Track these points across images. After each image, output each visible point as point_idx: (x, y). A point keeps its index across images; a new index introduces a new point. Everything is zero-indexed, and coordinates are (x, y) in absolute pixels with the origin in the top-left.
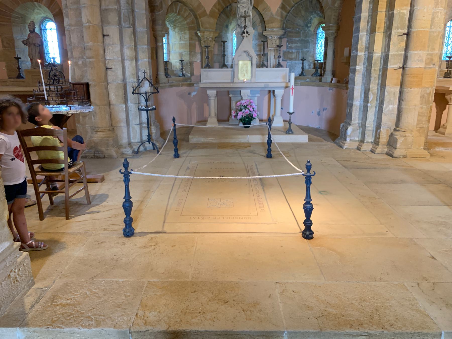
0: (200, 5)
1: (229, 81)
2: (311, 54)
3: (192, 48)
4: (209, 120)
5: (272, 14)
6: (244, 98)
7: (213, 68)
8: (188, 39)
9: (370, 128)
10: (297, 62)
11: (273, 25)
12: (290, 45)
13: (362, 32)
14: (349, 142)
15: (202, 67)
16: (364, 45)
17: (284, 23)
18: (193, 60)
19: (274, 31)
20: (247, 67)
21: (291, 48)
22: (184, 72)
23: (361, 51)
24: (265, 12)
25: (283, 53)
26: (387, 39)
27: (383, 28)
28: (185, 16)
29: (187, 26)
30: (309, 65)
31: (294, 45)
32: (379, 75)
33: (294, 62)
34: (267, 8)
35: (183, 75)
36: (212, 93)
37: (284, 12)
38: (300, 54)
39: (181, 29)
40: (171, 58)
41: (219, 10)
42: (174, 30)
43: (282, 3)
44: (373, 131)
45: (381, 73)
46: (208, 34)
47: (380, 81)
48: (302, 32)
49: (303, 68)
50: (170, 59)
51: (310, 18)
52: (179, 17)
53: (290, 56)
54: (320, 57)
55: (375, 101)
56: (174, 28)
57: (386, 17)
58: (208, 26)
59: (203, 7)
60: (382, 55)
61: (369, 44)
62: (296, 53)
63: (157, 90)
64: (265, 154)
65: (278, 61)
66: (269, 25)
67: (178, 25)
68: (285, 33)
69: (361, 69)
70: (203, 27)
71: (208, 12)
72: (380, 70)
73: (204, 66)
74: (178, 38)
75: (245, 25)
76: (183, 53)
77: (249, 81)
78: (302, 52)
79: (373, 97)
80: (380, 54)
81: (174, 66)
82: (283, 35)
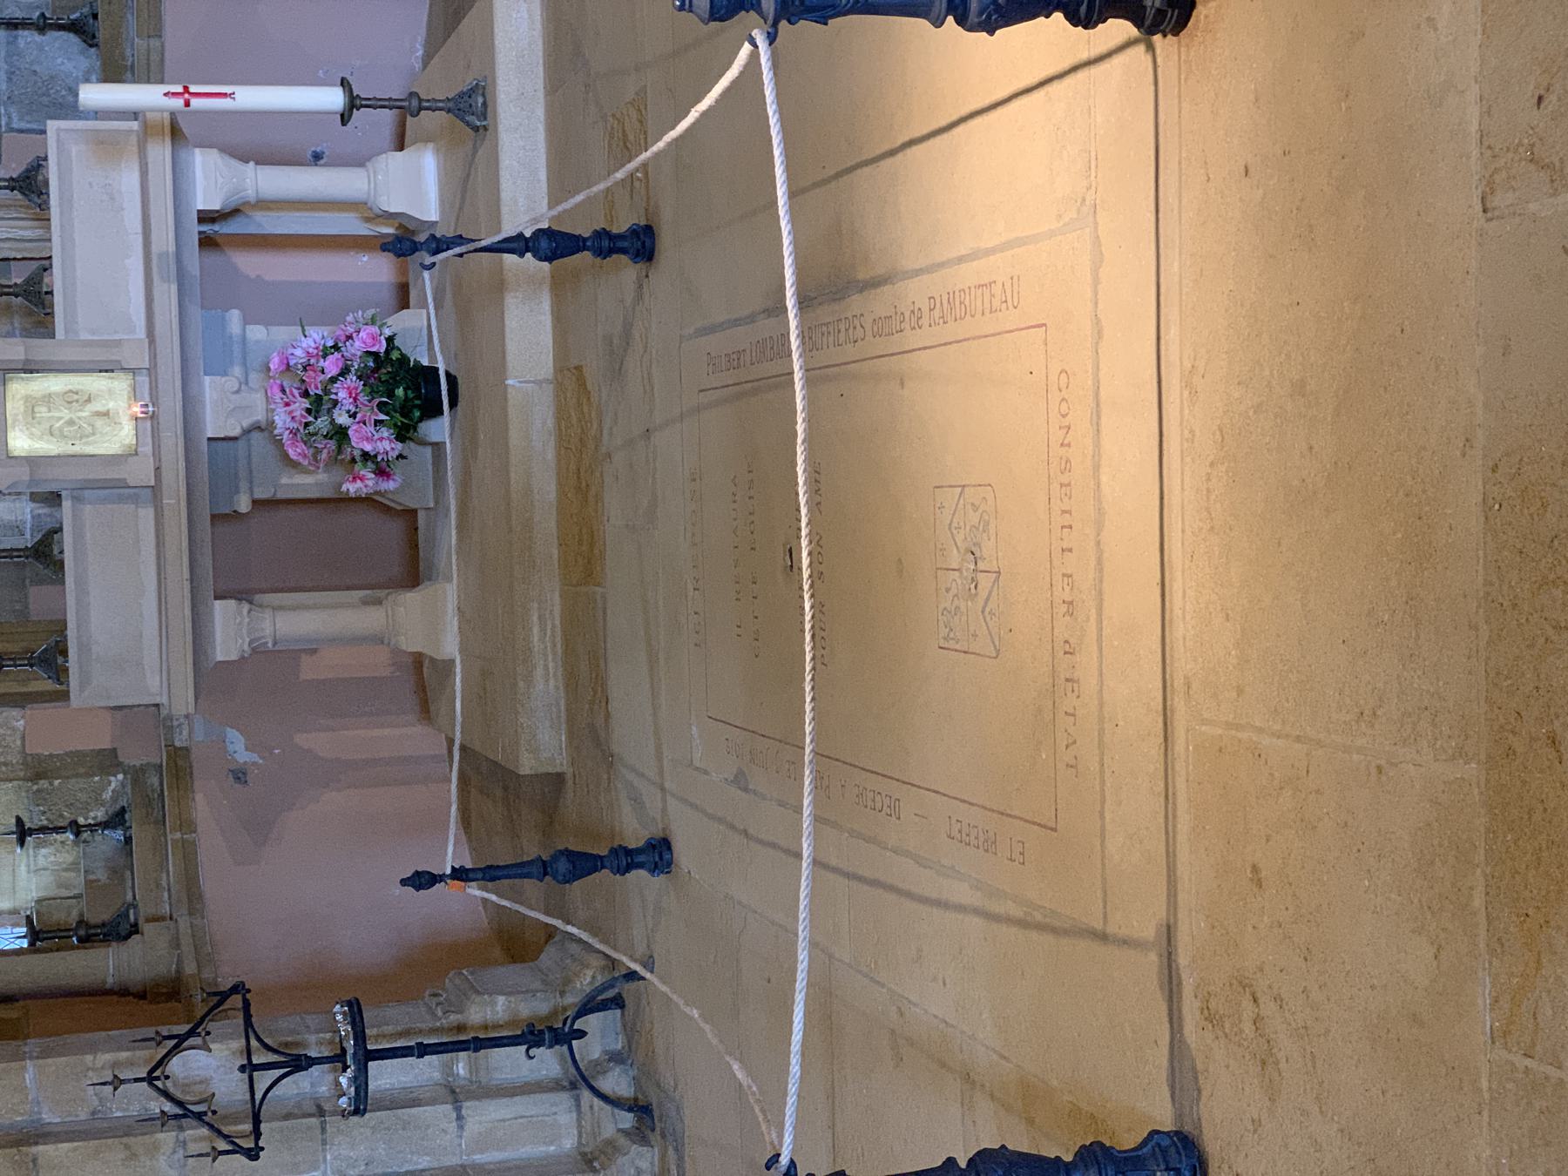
1: (147, 515)
6: (260, 416)
7: (63, 625)
15: (64, 696)
18: (14, 758)
20: (48, 399)
22: (99, 814)
35: (117, 819)
36: (231, 632)
50: (14, 912)
63: (224, 996)
64: (625, 270)
73: (49, 685)
77: (143, 379)
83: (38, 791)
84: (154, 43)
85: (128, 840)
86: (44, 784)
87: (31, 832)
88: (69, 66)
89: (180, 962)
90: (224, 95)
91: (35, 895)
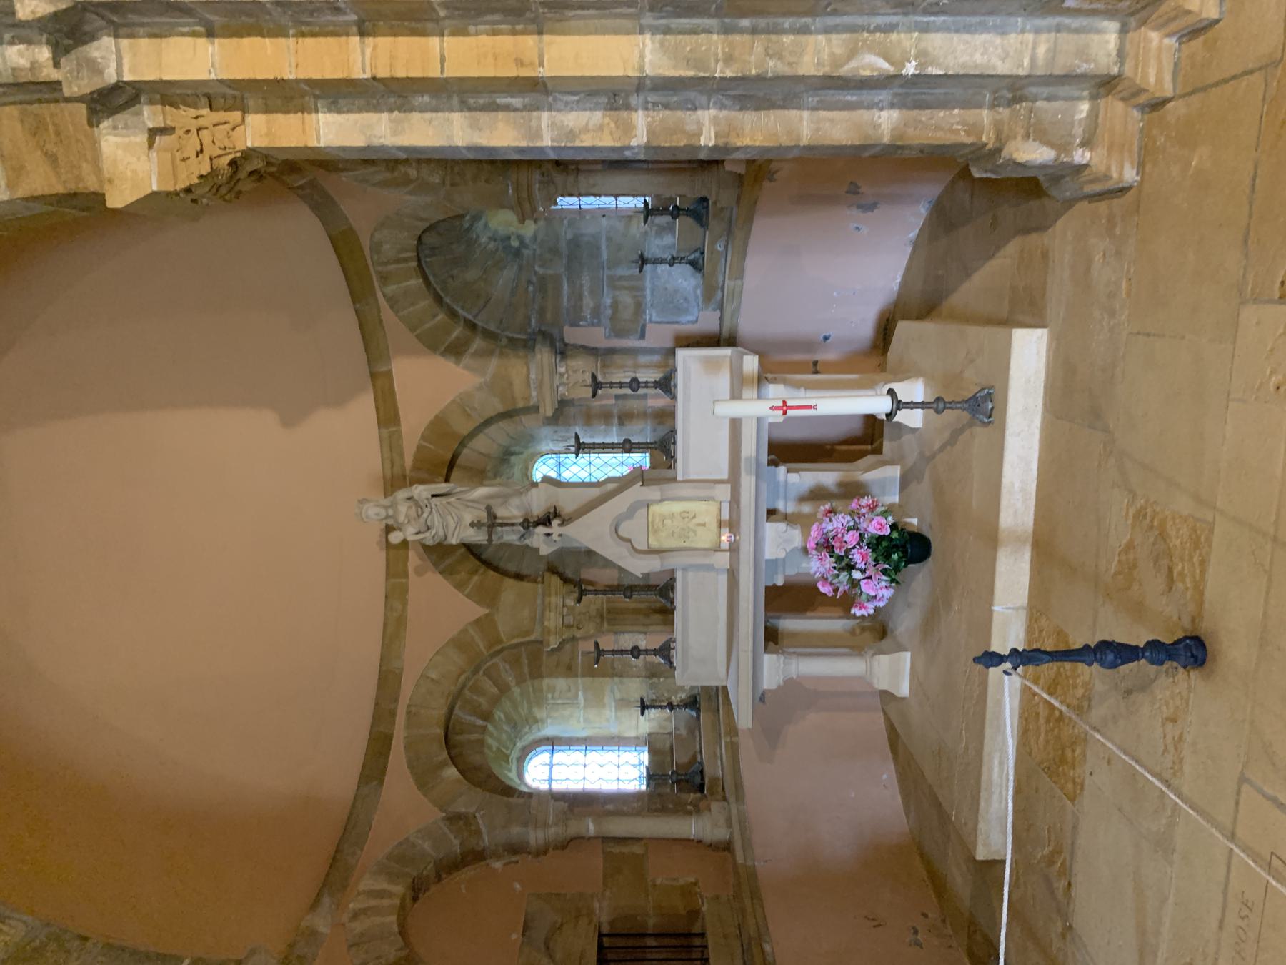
0: (460, 643)
2: (620, 226)
3: (600, 664)
5: (480, 388)
8: (570, 680)
9: (1042, 50)
10: (648, 284)
13: (538, 134)
14: (1102, 151)
16: (597, 117)
17: (511, 340)
19: (537, 376)
21: (596, 312)
23: (629, 128)
26: (571, 13)
27: (519, 38)
28: (495, 690)
29: (529, 683)
30: (662, 230)
31: (588, 302)
32: (754, 31)
34: (462, 404)
37: (472, 350)
38: (622, 271)
39: (539, 700)
40: (632, 734)
41: (475, 572)
42: (543, 721)
43: (443, 354)
44: (1058, 29)
45: (745, 23)
46: (552, 614)
47: (787, 23)
48: (540, 271)
49: (672, 262)
51: (492, 245)
52: (499, 714)
53: (627, 314)
54: (632, 203)
55: (894, 36)
56: (536, 721)
57: (464, 33)
58: (526, 613)
59: (464, 631)
60: (654, 30)
61: (592, 94)
62: (615, 288)
64: (1174, 684)
65: (651, 391)
67: (524, 711)
69: (715, 121)
70: (528, 633)
71: (482, 611)
72: (727, 30)
76: (618, 696)
78: (613, 263)
79: (871, 49)
80: (648, 36)
81: (661, 727)
82: (553, 345)
84: (739, 282)
86: (655, 680)
87: (648, 707)
88: (685, 284)
89: (731, 834)
90: (810, 407)
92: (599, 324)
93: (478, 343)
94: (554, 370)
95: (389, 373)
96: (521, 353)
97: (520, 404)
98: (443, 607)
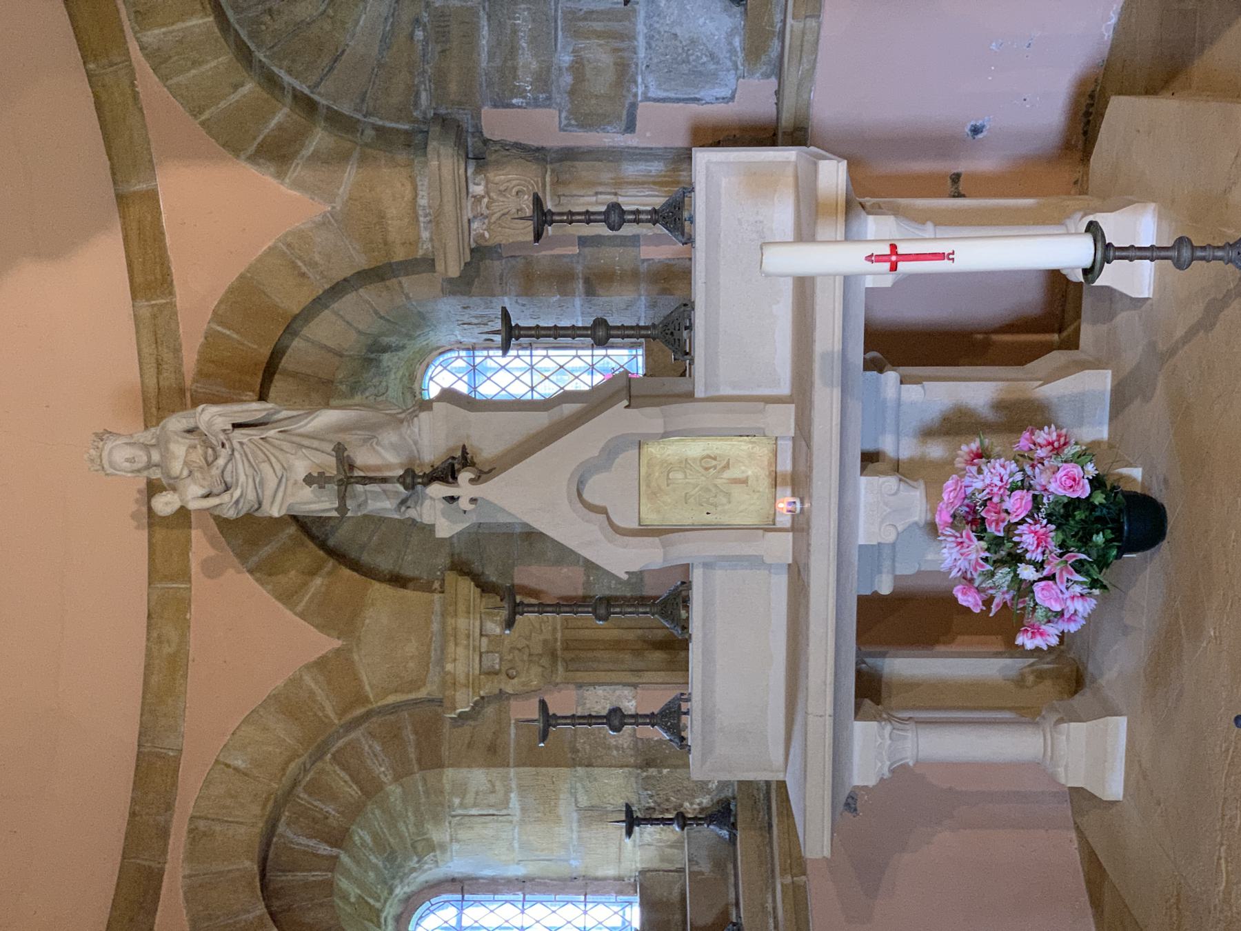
0: (288, 703)
4: (1073, 777)
5: (323, 224)
8: (495, 772)
11: (395, 212)
12: (525, 82)
17: (380, 130)
21: (543, 80)
24: (312, 264)
25: (583, 126)
28: (354, 791)
31: (527, 61)
33: (642, 53)
34: (290, 255)
39: (437, 809)
40: (611, 872)
41: (313, 573)
42: (443, 847)
46: (461, 651)
52: (361, 835)
53: (601, 84)
56: (431, 847)
58: (412, 648)
59: (295, 681)
62: (577, 34)
66: (393, 236)
67: (407, 828)
68: (444, 122)
70: (415, 685)
74: (490, 830)
75: (401, 480)
76: (584, 801)
82: (460, 143)
83: (647, 777)
84: (812, 23)
85: (733, 840)
86: (653, 771)
88: (711, 26)
91: (639, 866)
92: (548, 102)
93: (320, 138)
94: (463, 190)
95: (152, 196)
96: (402, 157)
97: (400, 255)
98: (258, 638)
